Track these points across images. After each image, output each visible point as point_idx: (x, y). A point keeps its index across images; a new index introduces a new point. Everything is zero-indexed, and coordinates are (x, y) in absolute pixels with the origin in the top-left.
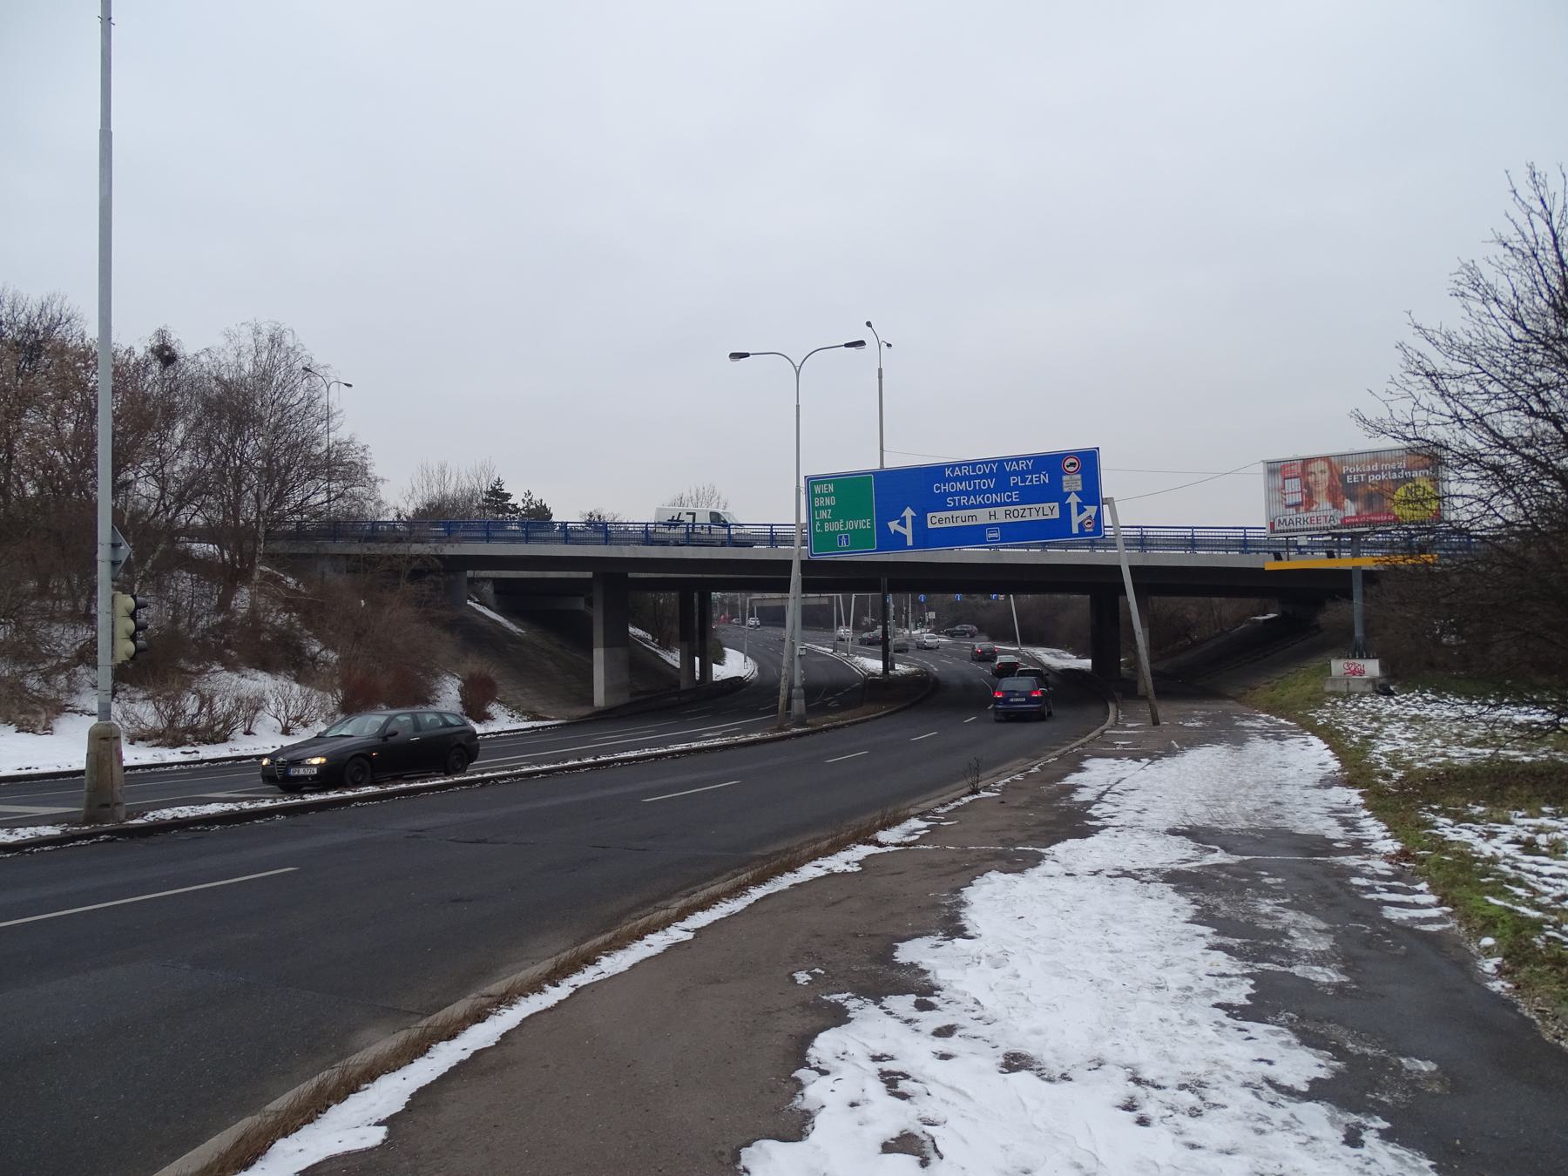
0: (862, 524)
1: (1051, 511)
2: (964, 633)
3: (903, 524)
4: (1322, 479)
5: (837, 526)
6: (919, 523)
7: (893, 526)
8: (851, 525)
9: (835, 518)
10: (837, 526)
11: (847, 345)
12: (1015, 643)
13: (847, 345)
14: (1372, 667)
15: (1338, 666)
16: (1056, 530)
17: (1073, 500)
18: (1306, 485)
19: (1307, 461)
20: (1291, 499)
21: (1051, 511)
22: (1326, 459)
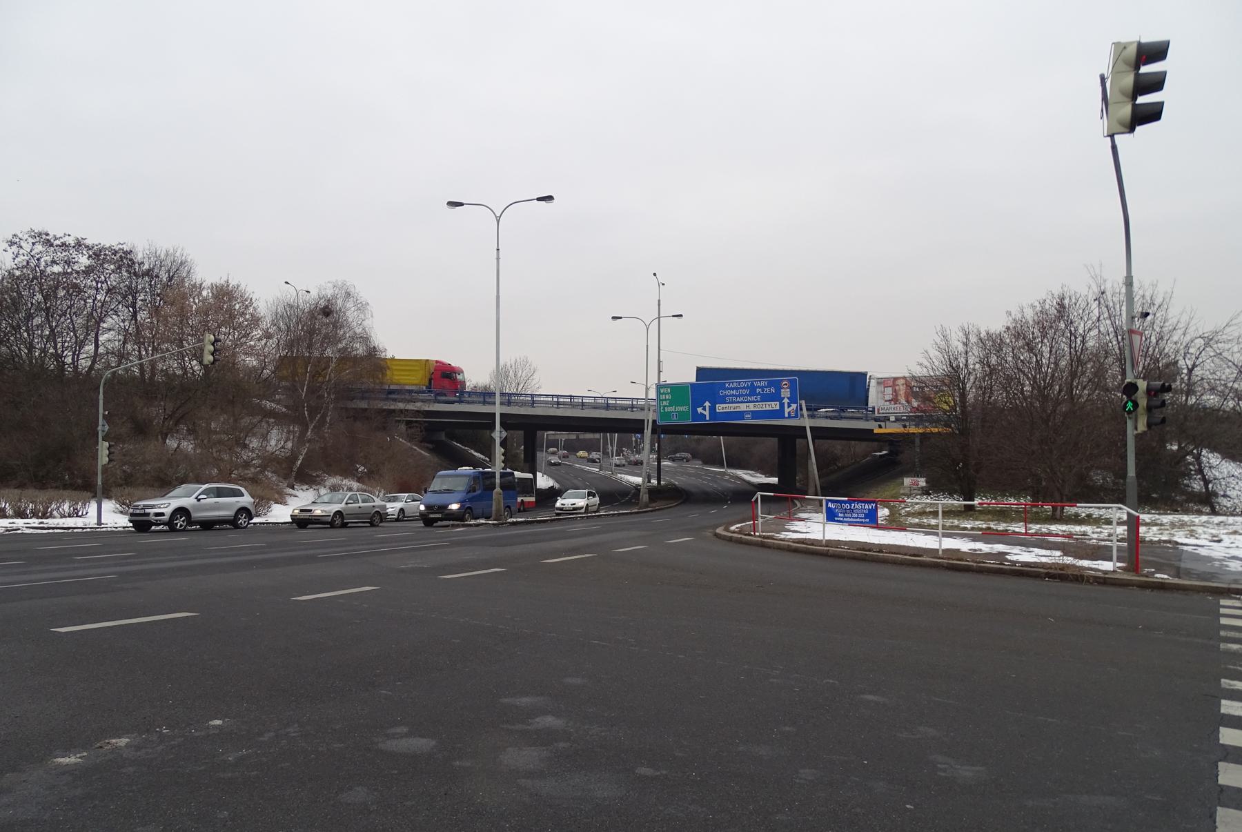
0: (685, 409)
1: (775, 406)
2: (682, 459)
3: (704, 409)
4: (902, 389)
5: (671, 409)
6: (712, 409)
7: (700, 410)
8: (679, 409)
9: (670, 405)
10: (671, 409)
11: (539, 199)
12: (722, 466)
13: (539, 199)
14: (922, 482)
15: (907, 481)
16: (779, 414)
17: (786, 401)
18: (895, 391)
19: (895, 379)
20: (887, 398)
21: (775, 406)
22: (904, 378)
